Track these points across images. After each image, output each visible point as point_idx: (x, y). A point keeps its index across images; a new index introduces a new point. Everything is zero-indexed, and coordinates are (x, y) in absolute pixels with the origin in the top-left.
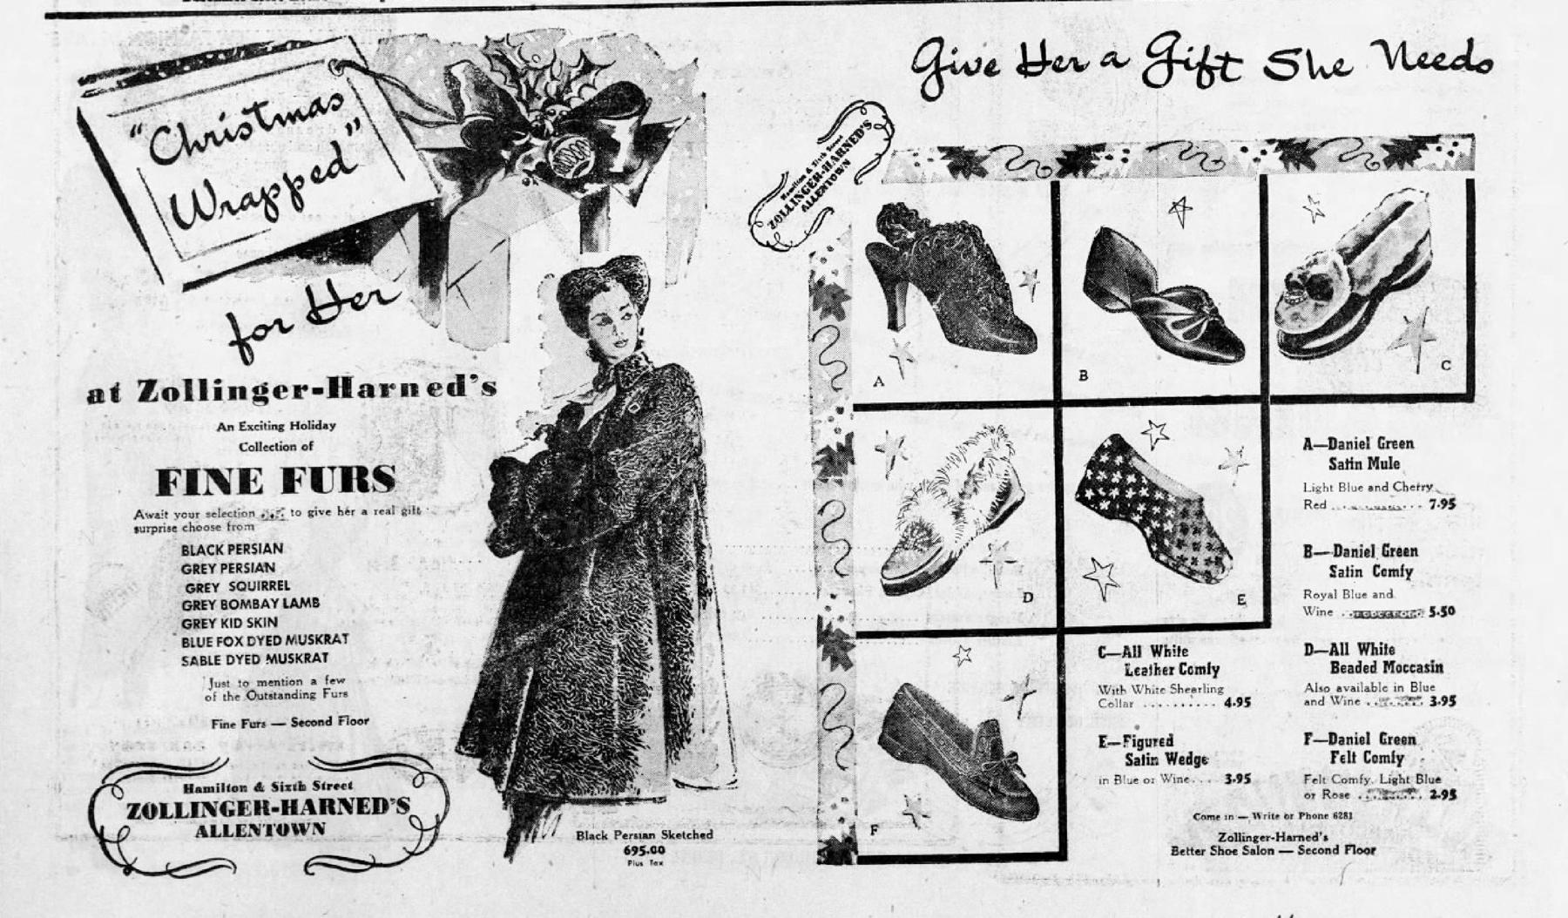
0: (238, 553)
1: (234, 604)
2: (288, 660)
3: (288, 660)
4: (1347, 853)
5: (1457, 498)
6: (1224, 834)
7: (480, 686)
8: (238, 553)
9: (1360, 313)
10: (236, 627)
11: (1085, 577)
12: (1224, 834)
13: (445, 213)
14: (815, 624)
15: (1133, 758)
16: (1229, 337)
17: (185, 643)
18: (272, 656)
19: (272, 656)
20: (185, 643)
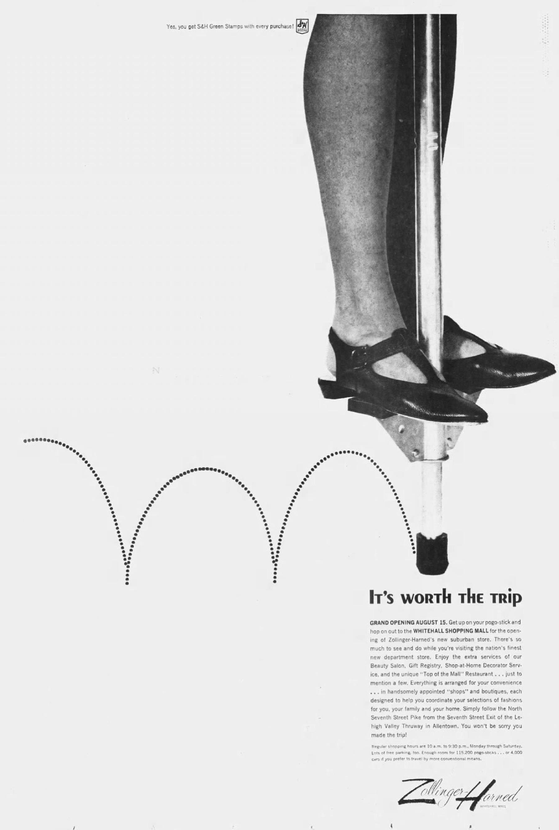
0: (399, 624)
1: (404, 692)
2: (432, 623)
3: (432, 623)
4: (406, 727)
5: (491, 723)
6: (391, 638)
7: (328, 233)
8: (399, 624)
9: (428, 101)
10: (386, 624)
11: (402, 802)
12: (391, 638)
13: (364, 213)
14: (382, 727)
15: (394, 665)
16: (421, 417)
17: (372, 666)
18: (477, 629)
19: (477, 629)
20: (372, 666)
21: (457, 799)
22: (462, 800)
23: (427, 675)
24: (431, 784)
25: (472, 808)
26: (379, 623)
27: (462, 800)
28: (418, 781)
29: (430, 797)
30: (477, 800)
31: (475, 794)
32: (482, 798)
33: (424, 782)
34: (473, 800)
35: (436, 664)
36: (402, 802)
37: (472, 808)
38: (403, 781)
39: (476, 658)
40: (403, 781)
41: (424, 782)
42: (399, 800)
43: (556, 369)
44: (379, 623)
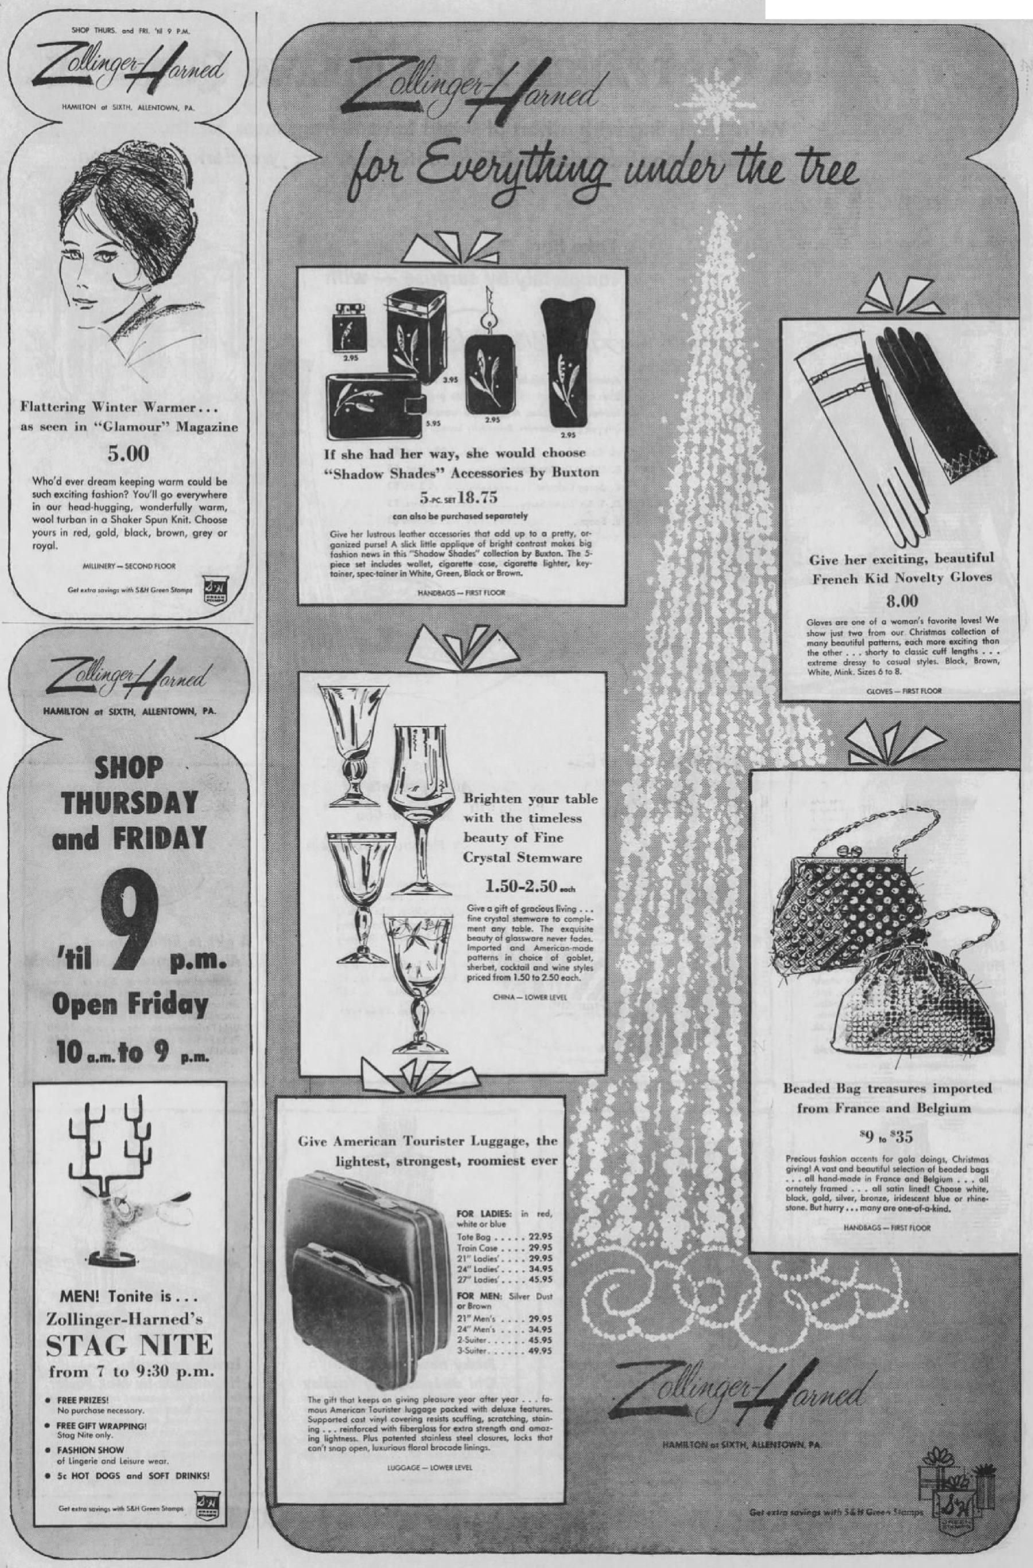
11: (350, 107)
21: (469, 102)
22: (479, 103)
23: (119, 1300)
24: (84, 49)
25: (500, 121)
26: (444, 593)
27: (479, 103)
28: (64, 46)
29: (84, 73)
30: (509, 103)
31: (156, 66)
32: (167, 74)
33: (397, 62)
34: (501, 103)
35: (408, 1158)
36: (350, 107)
37: (500, 121)
38: (39, 46)
39: (174, 957)
40: (39, 46)
41: (397, 62)
42: (34, 77)
43: (481, 418)
44: (444, 593)
